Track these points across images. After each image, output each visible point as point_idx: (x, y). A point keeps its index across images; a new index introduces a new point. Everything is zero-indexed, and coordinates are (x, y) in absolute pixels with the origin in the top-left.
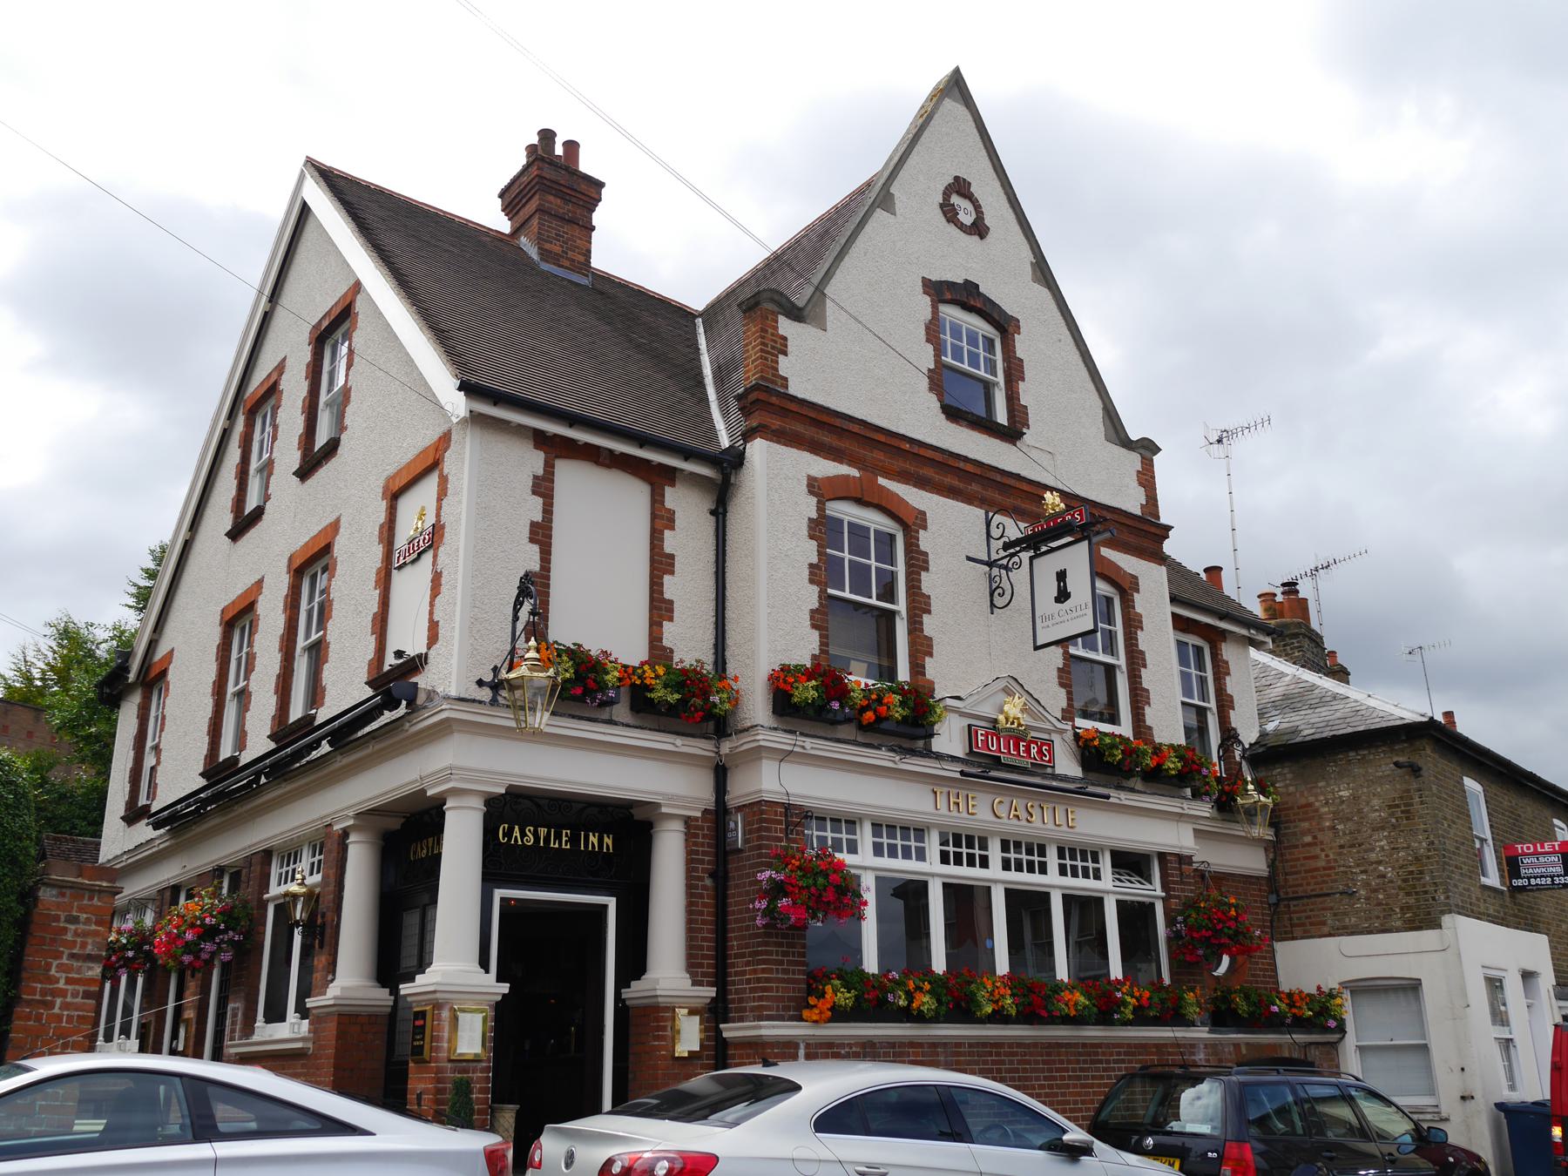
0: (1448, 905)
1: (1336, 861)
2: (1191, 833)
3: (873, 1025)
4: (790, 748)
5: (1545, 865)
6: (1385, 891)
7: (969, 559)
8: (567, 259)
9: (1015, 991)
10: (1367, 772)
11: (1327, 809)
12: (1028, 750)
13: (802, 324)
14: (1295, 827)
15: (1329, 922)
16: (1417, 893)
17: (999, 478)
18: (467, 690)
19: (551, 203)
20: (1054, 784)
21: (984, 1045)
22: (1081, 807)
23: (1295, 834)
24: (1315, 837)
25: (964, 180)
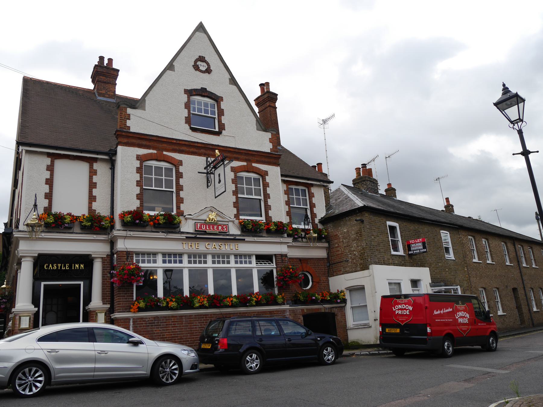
0: (371, 262)
1: (344, 251)
2: (287, 247)
3: (156, 312)
4: (126, 235)
5: (418, 246)
6: (356, 259)
7: (199, 173)
8: (107, 94)
9: (208, 299)
10: (351, 223)
11: (341, 236)
12: (218, 228)
13: (136, 110)
14: (334, 242)
15: (342, 270)
16: (363, 259)
17: (211, 147)
18: (24, 228)
19: (101, 78)
20: (228, 237)
21: (201, 315)
22: (240, 243)
23: (333, 244)
24: (338, 245)
25: (202, 56)
